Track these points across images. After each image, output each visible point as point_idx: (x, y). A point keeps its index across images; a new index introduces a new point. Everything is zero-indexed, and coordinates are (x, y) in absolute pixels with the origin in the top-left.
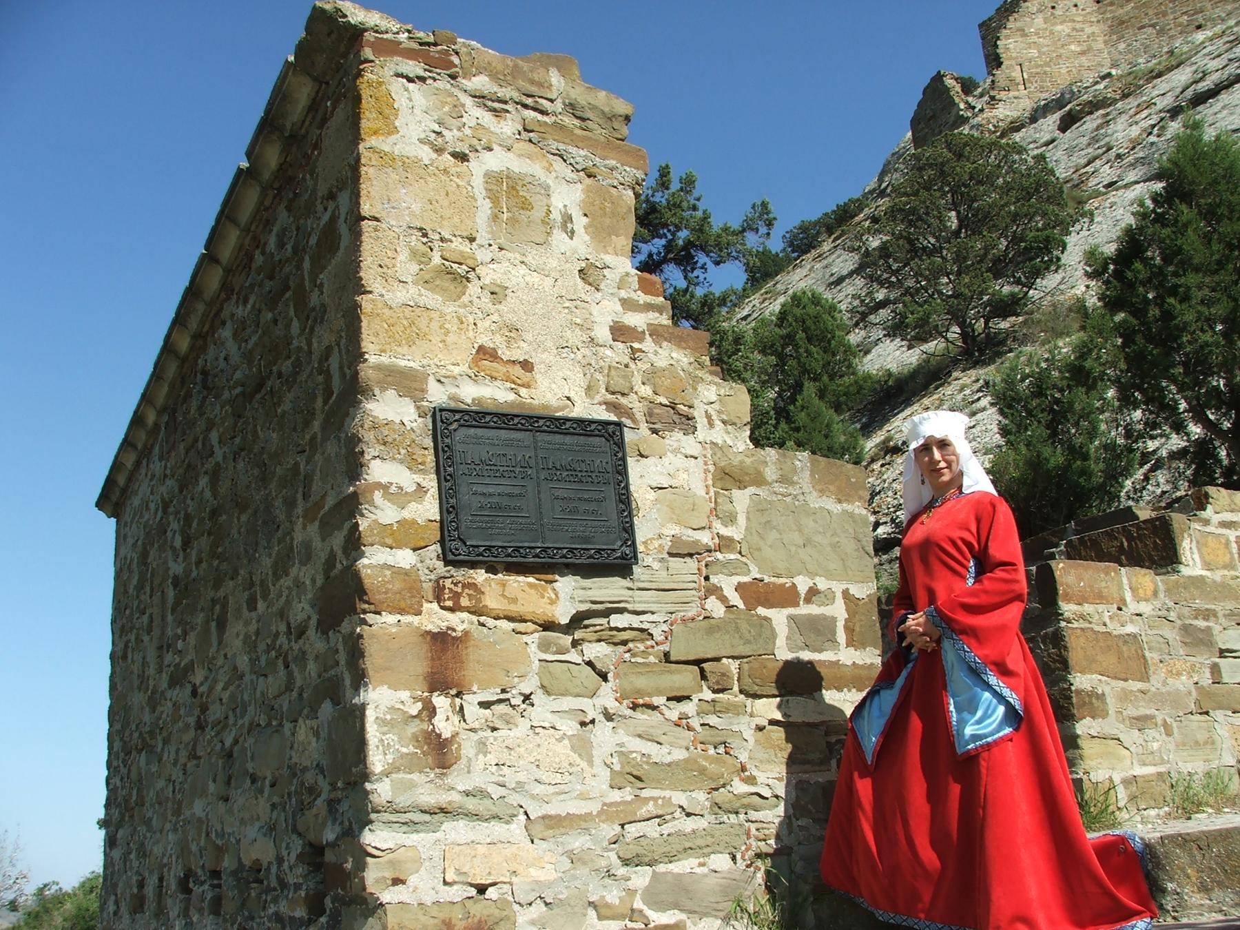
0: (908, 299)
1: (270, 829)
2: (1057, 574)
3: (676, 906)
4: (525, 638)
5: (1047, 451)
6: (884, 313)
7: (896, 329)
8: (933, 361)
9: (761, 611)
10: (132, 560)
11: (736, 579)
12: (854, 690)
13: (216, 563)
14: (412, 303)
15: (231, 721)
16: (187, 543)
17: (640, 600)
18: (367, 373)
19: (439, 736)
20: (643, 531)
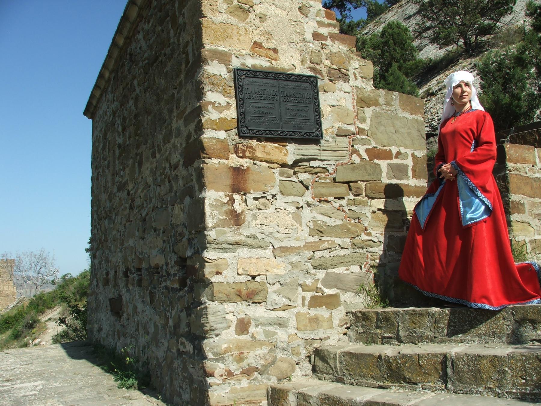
0: (441, 26)
1: (163, 251)
2: (506, 149)
3: (336, 287)
4: (273, 170)
5: (502, 96)
6: (430, 32)
7: (433, 41)
8: (451, 55)
9: (376, 161)
10: (100, 137)
11: (365, 147)
12: (415, 197)
13: (137, 138)
14: (224, 22)
15: (145, 205)
16: (124, 129)
17: (324, 155)
18: (205, 53)
19: (236, 212)
20: (325, 125)
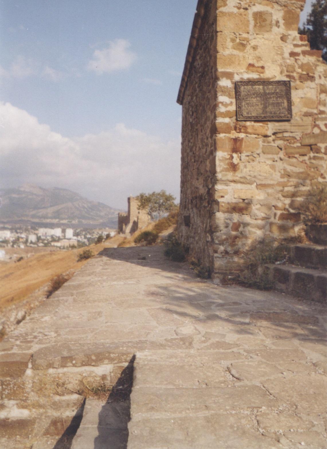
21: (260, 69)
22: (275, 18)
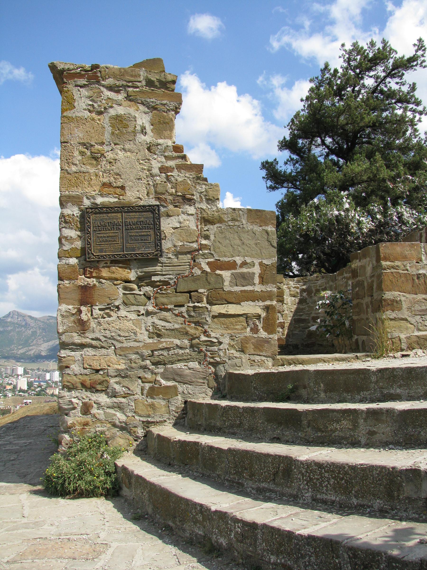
9: (218, 272)
21: (118, 191)
22: (139, 122)
